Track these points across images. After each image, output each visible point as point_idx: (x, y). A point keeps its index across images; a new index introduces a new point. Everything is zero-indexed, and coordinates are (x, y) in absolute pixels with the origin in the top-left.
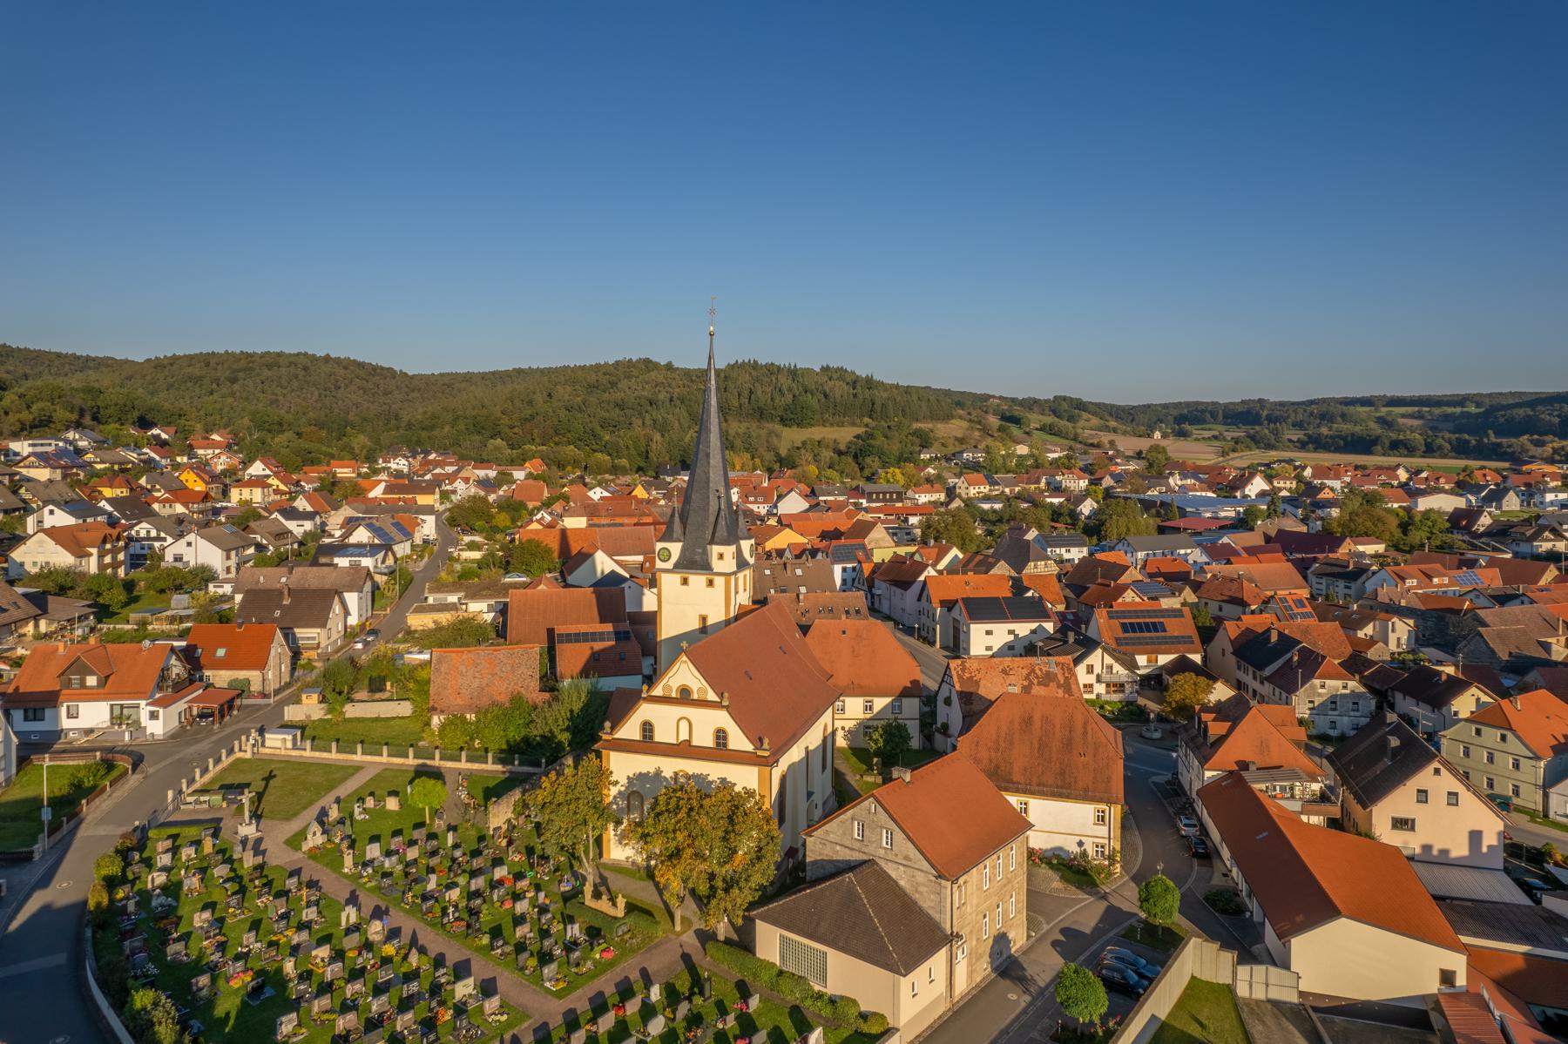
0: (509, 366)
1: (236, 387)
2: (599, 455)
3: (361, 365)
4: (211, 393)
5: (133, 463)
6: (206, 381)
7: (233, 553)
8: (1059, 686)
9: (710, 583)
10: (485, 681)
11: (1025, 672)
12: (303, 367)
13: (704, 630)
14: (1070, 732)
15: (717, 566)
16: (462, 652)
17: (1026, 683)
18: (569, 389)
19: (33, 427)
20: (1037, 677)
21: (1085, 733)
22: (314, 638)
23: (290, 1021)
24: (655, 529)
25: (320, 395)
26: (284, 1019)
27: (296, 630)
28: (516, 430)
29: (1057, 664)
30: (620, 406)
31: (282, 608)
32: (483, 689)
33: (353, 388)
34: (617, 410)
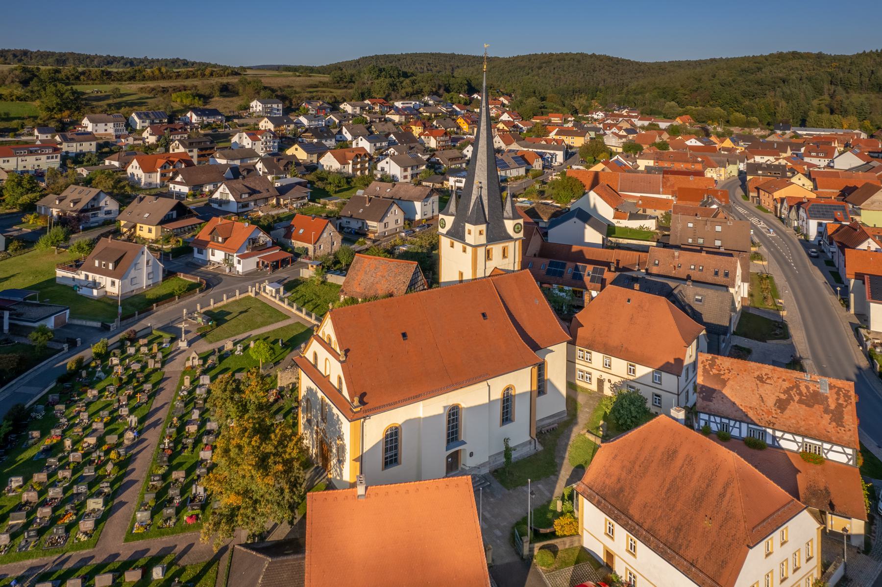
0: (708, 57)
1: (540, 71)
2: (737, 114)
3: (610, 59)
4: (528, 74)
5: (443, 113)
6: (527, 68)
7: (409, 169)
8: (827, 411)
9: (464, 251)
10: (377, 280)
11: (786, 385)
12: (578, 60)
13: (461, 281)
14: (708, 486)
15: (469, 239)
16: (371, 258)
17: (783, 397)
18: (726, 72)
19: (412, 95)
20: (801, 394)
21: (722, 495)
22: (376, 227)
23: (17, 481)
24: (663, 177)
25: (584, 75)
26: (13, 479)
27: (367, 222)
28: (686, 97)
29: (831, 387)
30: (759, 83)
31: (364, 208)
32: (373, 284)
33: (603, 71)
34: (756, 86)
